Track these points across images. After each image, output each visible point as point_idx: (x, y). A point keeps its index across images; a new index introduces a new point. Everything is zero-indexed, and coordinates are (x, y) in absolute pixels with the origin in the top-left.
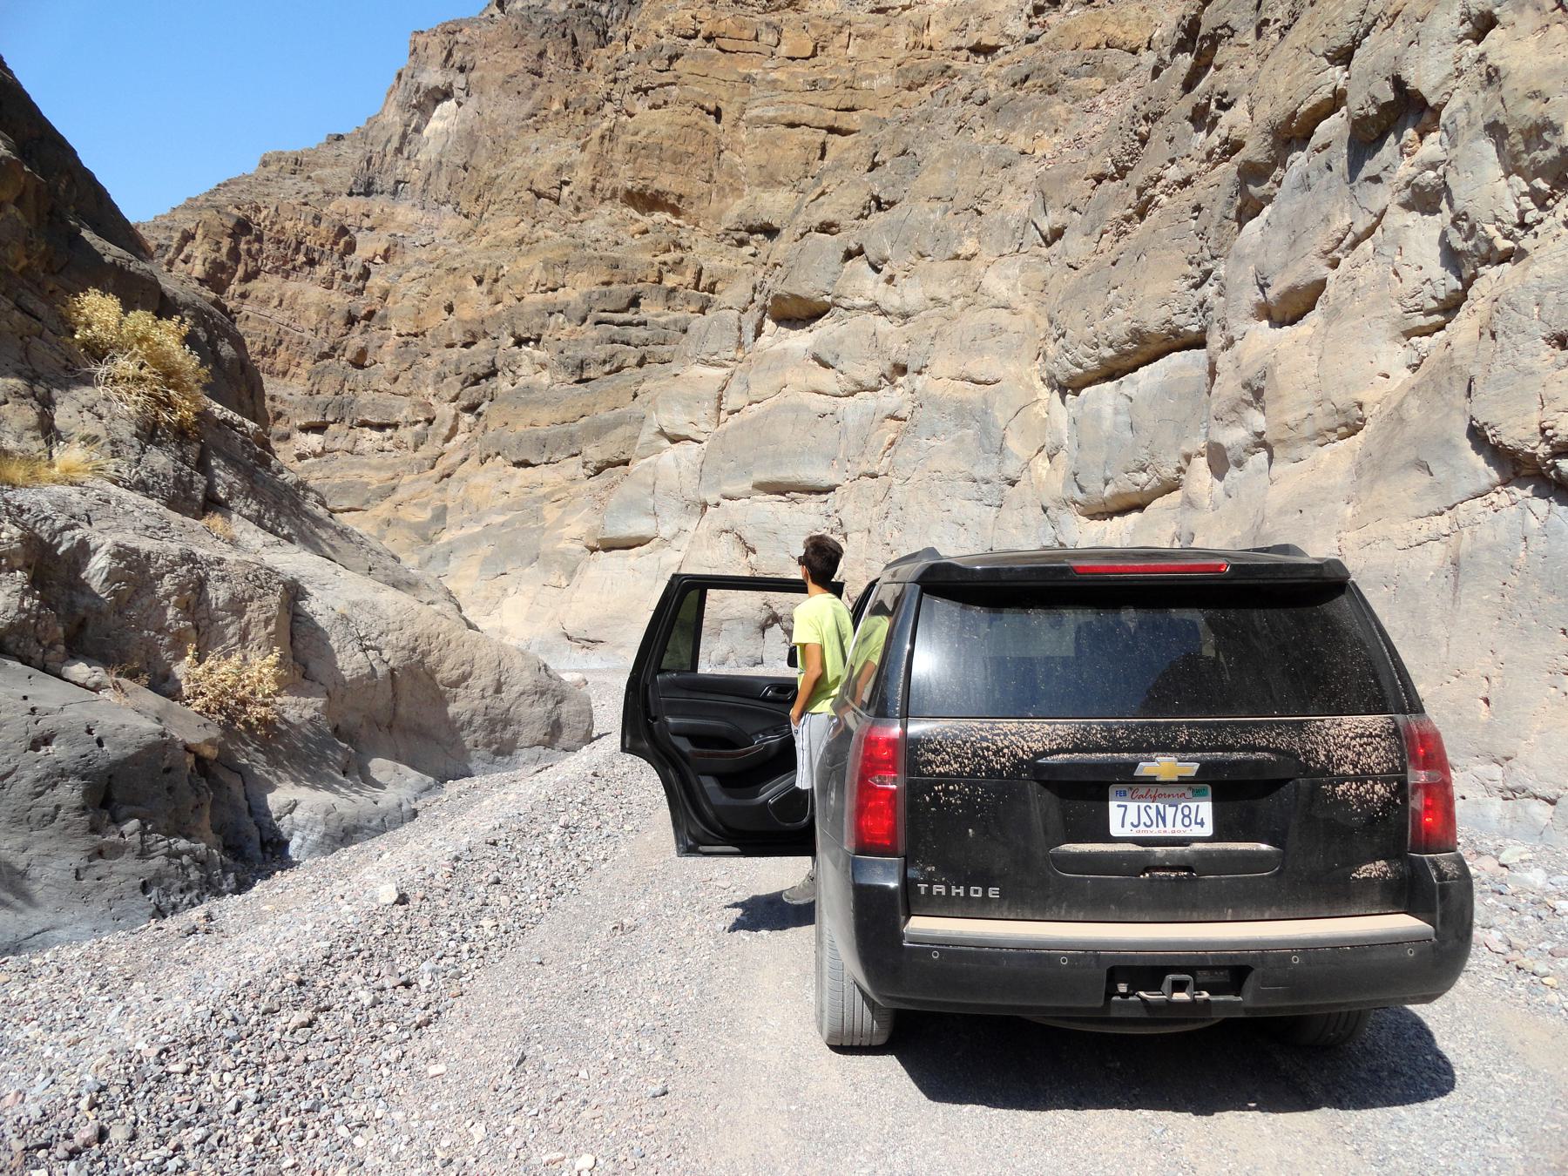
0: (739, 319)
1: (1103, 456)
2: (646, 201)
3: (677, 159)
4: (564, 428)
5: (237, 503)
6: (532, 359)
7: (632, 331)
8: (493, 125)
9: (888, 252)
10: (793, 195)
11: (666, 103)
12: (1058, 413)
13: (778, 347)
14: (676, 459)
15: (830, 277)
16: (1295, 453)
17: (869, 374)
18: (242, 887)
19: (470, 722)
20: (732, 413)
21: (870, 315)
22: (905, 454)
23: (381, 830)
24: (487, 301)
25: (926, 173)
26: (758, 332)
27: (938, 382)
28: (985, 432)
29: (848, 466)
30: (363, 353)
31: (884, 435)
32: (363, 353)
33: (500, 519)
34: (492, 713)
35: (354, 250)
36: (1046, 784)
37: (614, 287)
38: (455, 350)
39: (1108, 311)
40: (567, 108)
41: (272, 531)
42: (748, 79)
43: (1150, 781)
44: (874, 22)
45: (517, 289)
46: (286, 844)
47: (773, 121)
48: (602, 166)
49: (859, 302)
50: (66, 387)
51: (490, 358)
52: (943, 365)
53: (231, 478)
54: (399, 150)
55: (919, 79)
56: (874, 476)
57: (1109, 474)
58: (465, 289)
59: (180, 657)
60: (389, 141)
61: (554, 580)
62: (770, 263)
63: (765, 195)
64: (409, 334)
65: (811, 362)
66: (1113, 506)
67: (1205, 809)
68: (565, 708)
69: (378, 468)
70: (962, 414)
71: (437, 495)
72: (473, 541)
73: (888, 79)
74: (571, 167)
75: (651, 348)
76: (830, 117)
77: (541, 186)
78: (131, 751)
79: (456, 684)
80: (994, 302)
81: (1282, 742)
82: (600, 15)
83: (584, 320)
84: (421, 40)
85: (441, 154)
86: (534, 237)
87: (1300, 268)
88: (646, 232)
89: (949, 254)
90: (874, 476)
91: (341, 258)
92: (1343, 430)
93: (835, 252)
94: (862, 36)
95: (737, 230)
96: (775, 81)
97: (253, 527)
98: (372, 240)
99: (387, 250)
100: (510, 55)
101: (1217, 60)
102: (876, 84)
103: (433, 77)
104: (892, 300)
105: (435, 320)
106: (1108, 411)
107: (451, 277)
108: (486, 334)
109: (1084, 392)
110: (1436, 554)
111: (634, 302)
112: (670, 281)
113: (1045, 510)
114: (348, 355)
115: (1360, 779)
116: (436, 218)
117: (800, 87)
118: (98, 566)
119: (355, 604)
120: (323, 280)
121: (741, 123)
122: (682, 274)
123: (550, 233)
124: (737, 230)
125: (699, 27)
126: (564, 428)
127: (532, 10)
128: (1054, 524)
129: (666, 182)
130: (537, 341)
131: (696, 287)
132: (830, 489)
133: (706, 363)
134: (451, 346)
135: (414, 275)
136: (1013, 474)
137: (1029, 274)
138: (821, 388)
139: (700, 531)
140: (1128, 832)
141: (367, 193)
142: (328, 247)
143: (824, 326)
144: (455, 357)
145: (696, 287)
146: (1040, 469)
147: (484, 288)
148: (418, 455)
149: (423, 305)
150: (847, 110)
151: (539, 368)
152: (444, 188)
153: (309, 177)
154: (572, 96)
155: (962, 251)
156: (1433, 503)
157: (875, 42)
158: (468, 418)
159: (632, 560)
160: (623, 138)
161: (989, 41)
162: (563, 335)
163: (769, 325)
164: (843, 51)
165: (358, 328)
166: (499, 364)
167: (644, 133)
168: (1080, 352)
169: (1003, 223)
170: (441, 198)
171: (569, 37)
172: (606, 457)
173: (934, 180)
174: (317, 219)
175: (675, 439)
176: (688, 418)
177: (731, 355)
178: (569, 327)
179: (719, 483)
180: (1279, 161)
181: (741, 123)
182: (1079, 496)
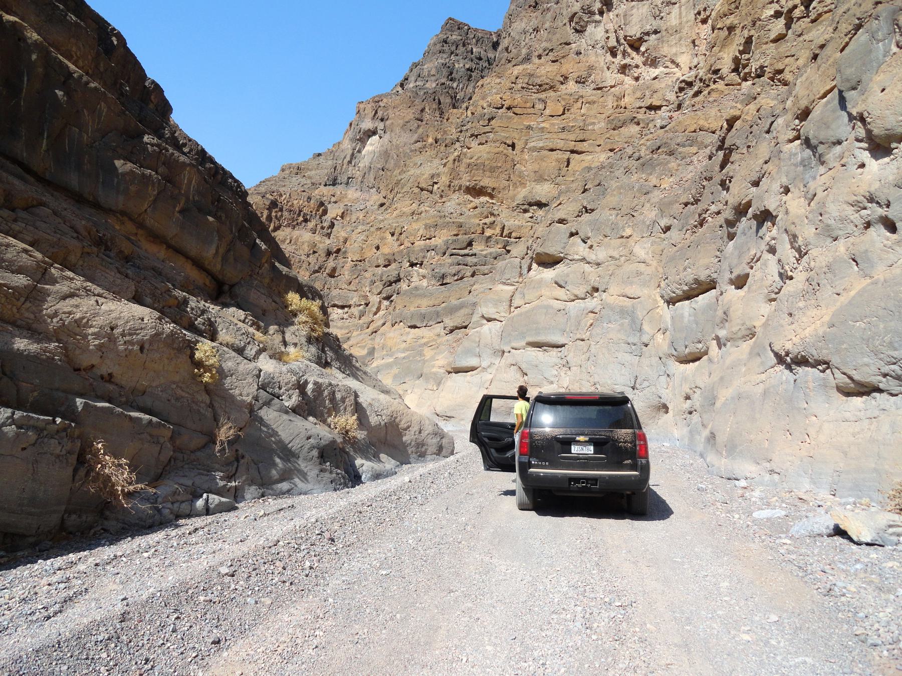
0: (520, 263)
1: (684, 335)
2: (476, 191)
3: (492, 170)
4: (434, 309)
5: (333, 363)
6: (418, 274)
7: (469, 259)
8: (397, 147)
9: (590, 234)
10: (552, 186)
11: (486, 142)
12: (665, 312)
13: (538, 277)
14: (490, 329)
15: (563, 245)
16: (737, 344)
17: (581, 291)
18: (353, 487)
19: (410, 444)
20: (516, 308)
21: (582, 263)
22: (597, 330)
23: (386, 476)
24: (396, 244)
25: (608, 196)
26: (530, 269)
27: (612, 297)
28: (633, 321)
29: (571, 335)
30: (334, 270)
31: (587, 321)
32: (334, 270)
33: (403, 355)
34: (418, 441)
35: (326, 213)
36: (558, 441)
37: (459, 237)
38: (380, 268)
39: (685, 269)
40: (436, 142)
41: (344, 373)
42: (529, 128)
43: (579, 441)
44: (595, 95)
45: (411, 239)
46: (361, 477)
47: (542, 148)
48: (454, 174)
49: (576, 257)
50: (287, 327)
51: (397, 272)
52: (614, 289)
53: (332, 354)
54: (350, 162)
55: (619, 124)
56: (583, 340)
57: (687, 343)
58: (385, 238)
59: (330, 416)
60: (345, 158)
61: (430, 387)
62: (535, 237)
63: (538, 186)
64: (357, 261)
65: (554, 285)
66: (690, 358)
67: (592, 448)
68: (444, 441)
69: (341, 328)
70: (623, 312)
71: (370, 342)
72: (389, 366)
73: (603, 124)
74: (438, 175)
75: (478, 267)
76: (571, 145)
77: (423, 185)
78: (327, 442)
79: (405, 429)
80: (638, 260)
81: (608, 434)
82: (453, 88)
83: (444, 254)
84: (362, 106)
85: (371, 163)
86: (420, 211)
87: (741, 268)
88: (476, 207)
89: (618, 236)
90: (583, 340)
91: (320, 218)
92: (751, 336)
93: (565, 233)
94: (589, 103)
95: (523, 204)
96: (543, 128)
97: (339, 371)
98: (336, 208)
99: (343, 213)
100: (406, 111)
101: (731, 159)
102: (596, 127)
103: (368, 125)
104: (592, 257)
105: (370, 253)
106: (686, 314)
107: (379, 232)
108: (395, 260)
109: (677, 304)
110: (760, 389)
111: (470, 244)
112: (488, 233)
113: (660, 358)
114: (327, 271)
115: (625, 442)
116: (368, 196)
117: (556, 130)
118: (310, 386)
119: (373, 400)
120: (311, 230)
121: (525, 150)
122: (494, 229)
123: (428, 209)
124: (523, 204)
125: (504, 103)
126: (434, 309)
127: (418, 88)
128: (665, 365)
129: (486, 182)
130: (421, 264)
131: (501, 236)
132: (563, 346)
133: (504, 283)
134: (378, 266)
135: (360, 231)
136: (646, 341)
137: (655, 247)
138: (558, 298)
139: (501, 364)
140: (575, 452)
141: (334, 184)
142: (314, 212)
143: (560, 268)
144: (380, 272)
145: (501, 236)
146: (659, 339)
147: (395, 237)
148: (361, 322)
149: (364, 246)
150: (581, 141)
151: (421, 278)
152: (372, 180)
153: (304, 176)
154: (439, 136)
155: (625, 234)
156: (762, 370)
157: (595, 105)
158: (386, 303)
159: (468, 377)
160: (464, 160)
161: (658, 103)
162: (434, 261)
163: (535, 266)
164: (579, 111)
165: (332, 257)
166: (402, 276)
167: (475, 158)
168: (674, 286)
169: (644, 222)
170: (371, 185)
171: (437, 101)
172: (455, 324)
173: (612, 199)
174: (309, 198)
175: (489, 320)
176: (496, 310)
177: (516, 280)
178: (437, 258)
179: (510, 342)
180: (738, 220)
181: (525, 150)
182: (675, 353)
